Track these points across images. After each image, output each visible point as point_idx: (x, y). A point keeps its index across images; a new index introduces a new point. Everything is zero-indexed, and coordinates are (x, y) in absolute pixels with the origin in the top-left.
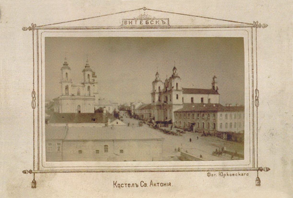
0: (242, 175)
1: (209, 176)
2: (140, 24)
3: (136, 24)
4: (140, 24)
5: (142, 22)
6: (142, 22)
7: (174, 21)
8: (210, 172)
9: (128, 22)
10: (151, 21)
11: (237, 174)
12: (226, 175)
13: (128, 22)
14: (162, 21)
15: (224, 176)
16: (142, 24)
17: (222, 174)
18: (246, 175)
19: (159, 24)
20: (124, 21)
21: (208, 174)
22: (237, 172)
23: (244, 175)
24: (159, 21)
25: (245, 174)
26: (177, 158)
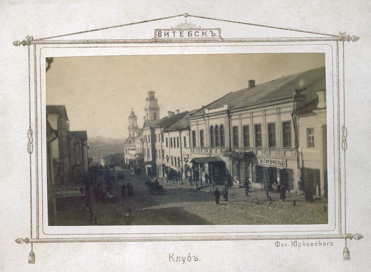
4: (181, 36)
8: (279, 241)
11: (317, 243)
12: (302, 245)
17: (295, 243)
20: (157, 31)
22: (317, 241)
23: (326, 244)
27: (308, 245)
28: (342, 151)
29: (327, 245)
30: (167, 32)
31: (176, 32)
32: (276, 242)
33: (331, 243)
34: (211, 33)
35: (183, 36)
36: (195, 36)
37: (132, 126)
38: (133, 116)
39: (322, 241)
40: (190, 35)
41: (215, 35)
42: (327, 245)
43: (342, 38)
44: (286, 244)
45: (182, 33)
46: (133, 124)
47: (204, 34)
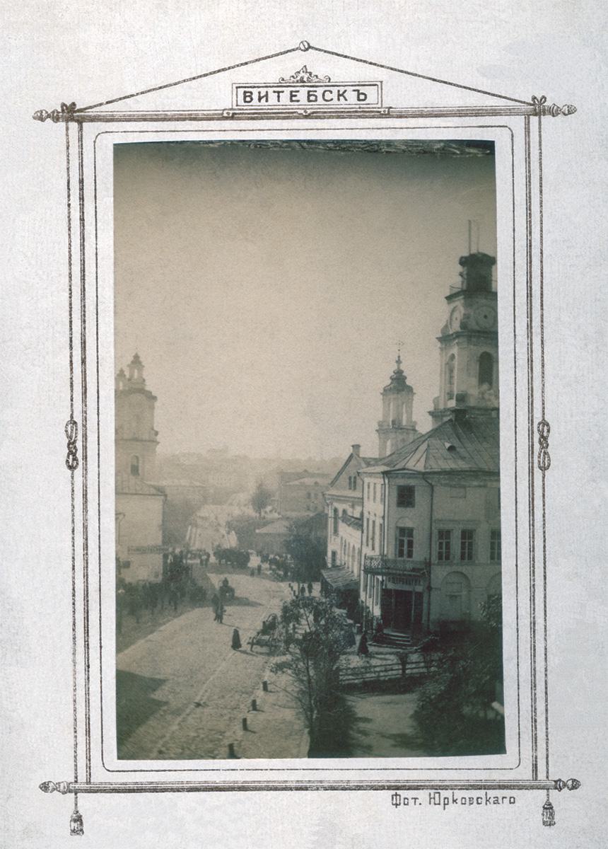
0: (497, 802)
1: (397, 805)
2: (292, 101)
3: (279, 101)
4: (292, 101)
5: (295, 96)
6: (295, 96)
7: (400, 94)
8: (398, 792)
9: (255, 96)
10: (325, 91)
11: (481, 798)
12: (451, 801)
13: (255, 96)
14: (354, 91)
15: (445, 804)
16: (298, 101)
17: (437, 795)
18: (506, 801)
19: (346, 100)
20: (241, 91)
21: (398, 803)
22: (481, 793)
23: (500, 801)
24: (345, 91)
25: (506, 798)
26: (485, 386)
27: (446, 800)
28: (78, 418)
29: (503, 802)
30: (342, 89)
31: (283, 92)
32: (393, 796)
33: (511, 798)
34: (356, 92)
35: (298, 101)
36: (243, 101)
37: (393, 422)
38: (399, 385)
39: (492, 793)
40: (362, 97)
41: (366, 98)
42: (503, 802)
43: (538, 108)
44: (415, 799)
45: (294, 93)
46: (399, 414)
47: (341, 98)
